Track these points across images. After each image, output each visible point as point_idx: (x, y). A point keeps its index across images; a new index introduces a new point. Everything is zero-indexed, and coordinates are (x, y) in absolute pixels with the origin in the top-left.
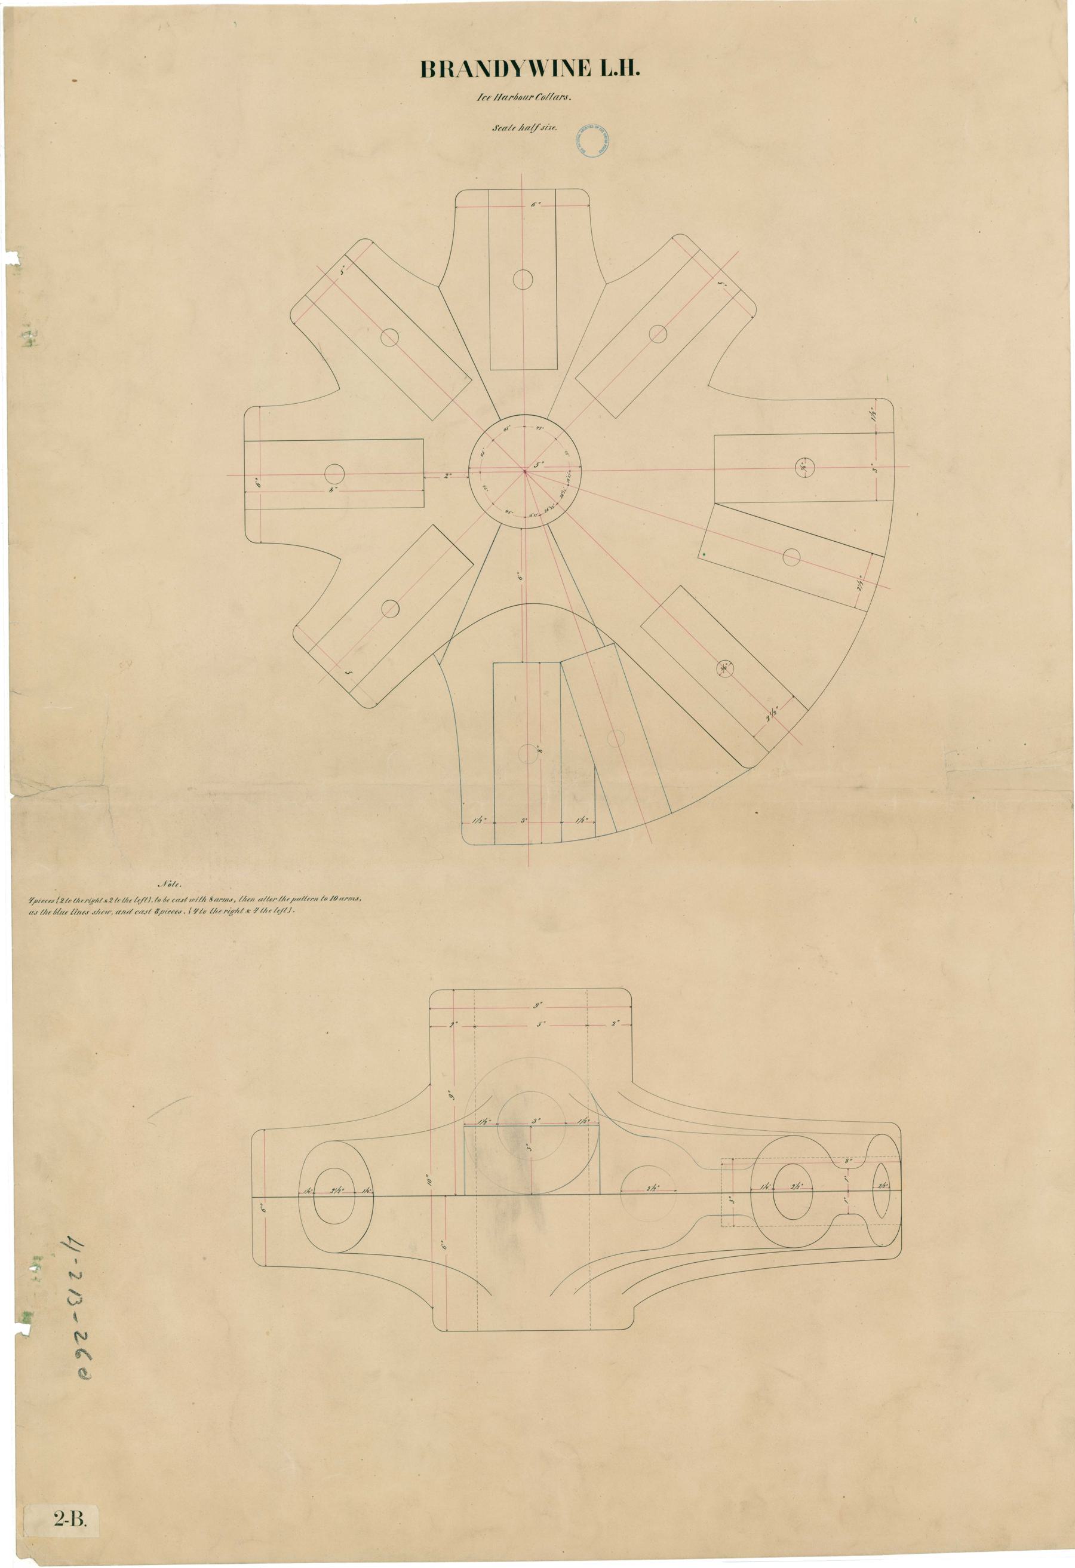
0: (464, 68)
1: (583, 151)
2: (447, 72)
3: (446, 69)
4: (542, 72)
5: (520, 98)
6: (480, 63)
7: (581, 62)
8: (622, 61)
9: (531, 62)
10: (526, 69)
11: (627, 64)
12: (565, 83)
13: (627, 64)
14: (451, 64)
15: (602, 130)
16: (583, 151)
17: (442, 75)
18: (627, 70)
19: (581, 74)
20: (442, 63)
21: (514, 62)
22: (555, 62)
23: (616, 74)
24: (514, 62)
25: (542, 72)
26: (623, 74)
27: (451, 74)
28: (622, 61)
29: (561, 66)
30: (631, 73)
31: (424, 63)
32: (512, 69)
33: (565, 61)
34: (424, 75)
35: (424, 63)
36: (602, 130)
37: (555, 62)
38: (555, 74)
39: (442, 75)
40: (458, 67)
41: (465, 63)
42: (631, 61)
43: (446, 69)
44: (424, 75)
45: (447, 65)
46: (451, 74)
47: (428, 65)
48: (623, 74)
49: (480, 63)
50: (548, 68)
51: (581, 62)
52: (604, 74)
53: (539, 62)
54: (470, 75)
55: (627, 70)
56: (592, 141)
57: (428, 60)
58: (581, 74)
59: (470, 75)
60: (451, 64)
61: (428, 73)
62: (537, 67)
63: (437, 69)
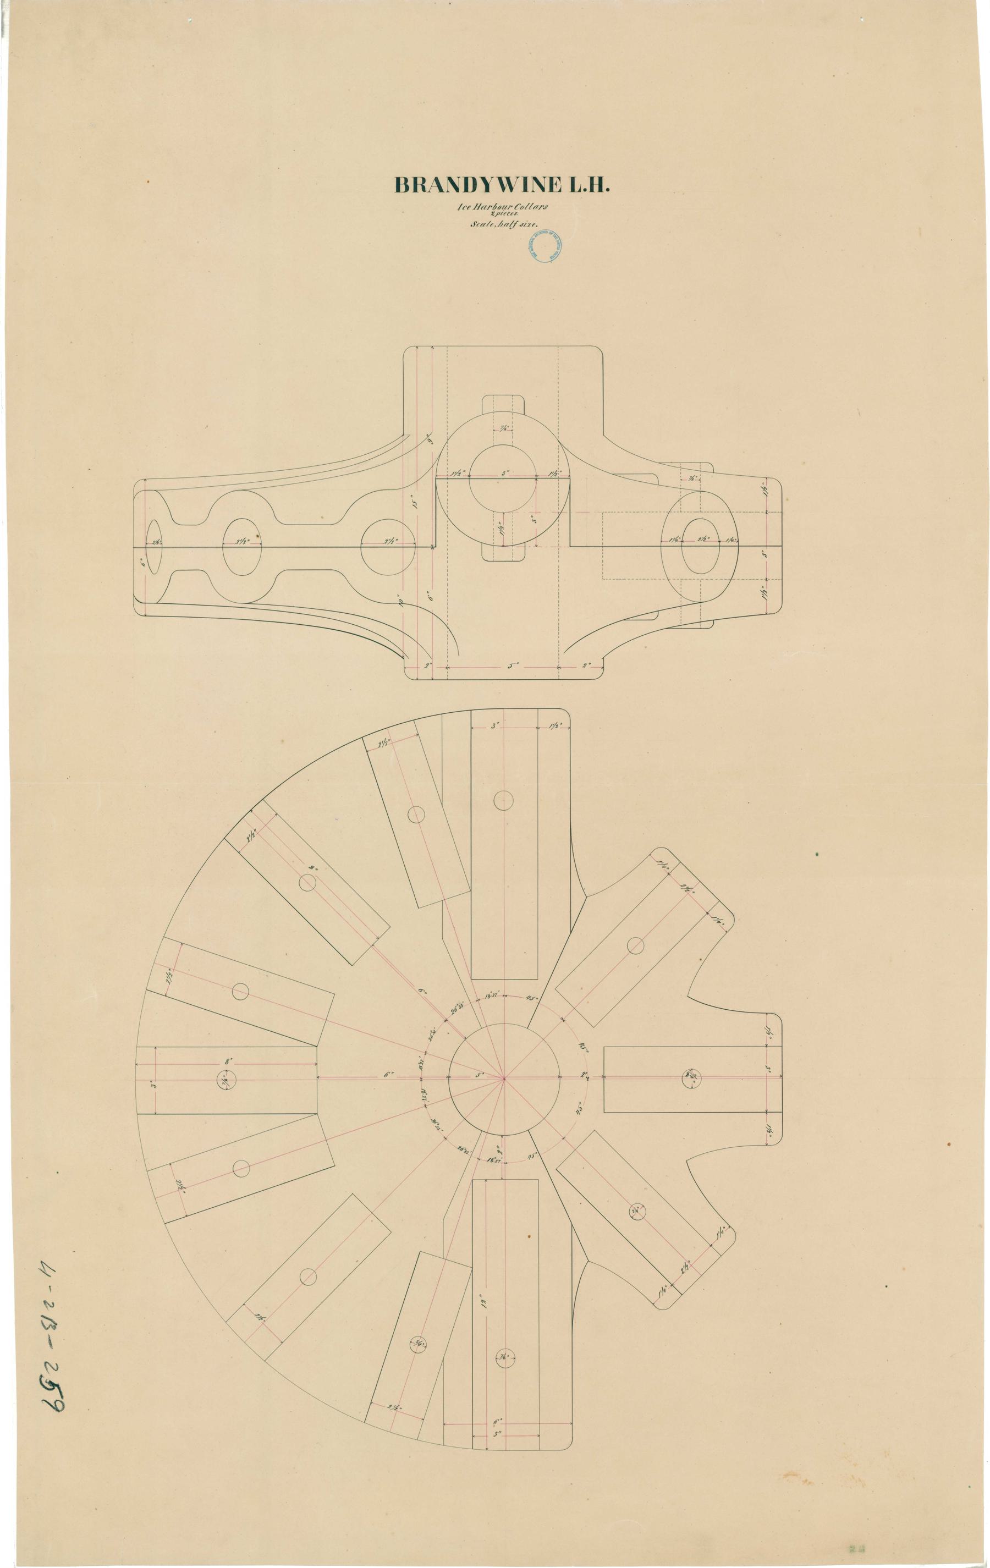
0: (435, 184)
1: (535, 255)
2: (419, 188)
3: (418, 185)
7: (551, 179)
8: (592, 179)
9: (500, 179)
10: (494, 185)
11: (596, 181)
13: (596, 181)
14: (424, 180)
15: (556, 236)
16: (535, 255)
17: (415, 190)
18: (596, 188)
19: (551, 190)
20: (415, 179)
21: (484, 179)
22: (525, 179)
23: (585, 190)
24: (484, 179)
25: (511, 189)
26: (592, 190)
27: (424, 189)
28: (592, 179)
30: (600, 190)
32: (480, 185)
34: (398, 190)
35: (398, 179)
36: (556, 236)
37: (525, 179)
38: (525, 190)
39: (415, 190)
41: (436, 179)
42: (600, 179)
43: (418, 185)
44: (398, 190)
45: (420, 181)
46: (424, 189)
47: (402, 181)
48: (592, 190)
49: (450, 179)
50: (518, 185)
51: (551, 179)
52: (573, 190)
54: (441, 190)
55: (596, 188)
58: (551, 190)
59: (441, 190)
60: (424, 180)
61: (403, 188)
62: (506, 184)
63: (411, 184)
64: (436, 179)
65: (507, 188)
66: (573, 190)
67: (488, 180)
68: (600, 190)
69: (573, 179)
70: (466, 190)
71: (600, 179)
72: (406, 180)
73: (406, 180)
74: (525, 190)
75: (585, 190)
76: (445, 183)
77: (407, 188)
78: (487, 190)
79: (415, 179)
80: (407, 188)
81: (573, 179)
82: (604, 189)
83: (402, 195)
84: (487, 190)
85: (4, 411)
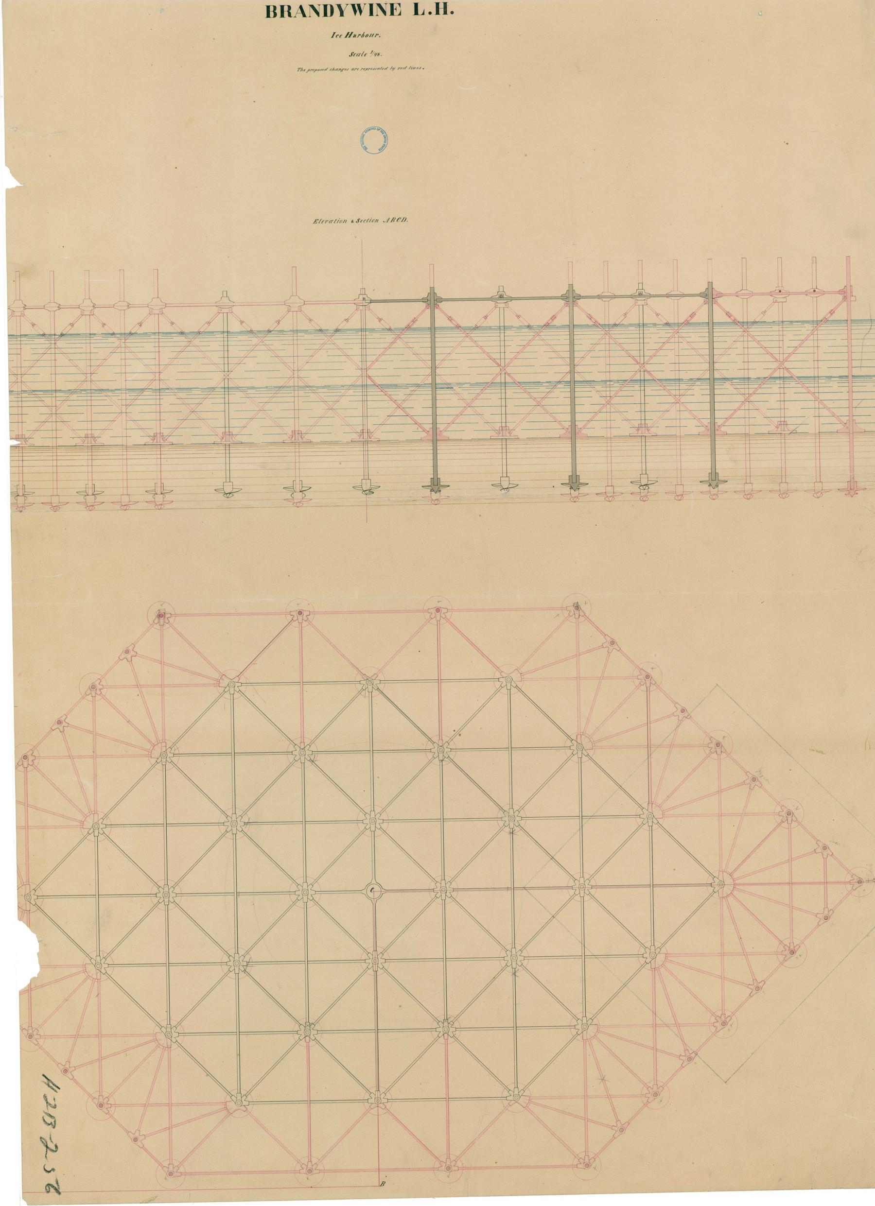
0: (300, 11)
1: (366, 148)
2: (286, 14)
3: (285, 11)
4: (361, 12)
5: (367, 36)
6: (312, 6)
7: (392, 5)
8: (437, 4)
9: (353, 5)
10: (348, 11)
11: (441, 6)
12: (380, 21)
13: (441, 6)
14: (289, 7)
15: (383, 132)
16: (366, 148)
17: (282, 16)
18: (441, 11)
19: (392, 14)
20: (282, 7)
21: (339, 6)
22: (371, 5)
23: (430, 13)
24: (339, 6)
25: (361, 12)
26: (438, 13)
27: (290, 15)
28: (437, 4)
29: (376, 8)
30: (445, 13)
31: (268, 7)
32: (337, 11)
33: (379, 5)
34: (268, 16)
35: (268, 7)
36: (383, 132)
37: (371, 5)
38: (371, 14)
39: (282, 16)
40: (295, 10)
41: (301, 7)
42: (445, 4)
43: (285, 11)
44: (268, 16)
45: (286, 9)
46: (290, 15)
47: (272, 9)
48: (438, 13)
49: (312, 6)
50: (366, 10)
51: (392, 5)
52: (416, 13)
53: (359, 5)
54: (304, 16)
55: (441, 11)
56: (374, 140)
57: (271, 3)
58: (392, 14)
59: (304, 16)
60: (289, 7)
61: (272, 14)
62: (357, 9)
63: (278, 11)
64: (301, 7)
65: (358, 12)
66: (416, 13)
67: (343, 7)
68: (445, 13)
69: (416, 5)
70: (325, 15)
71: (445, 4)
72: (275, 7)
73: (275, 7)
74: (371, 14)
75: (430, 13)
76: (307, 10)
77: (275, 15)
78: (342, 14)
79: (282, 7)
80: (275, 15)
81: (416, 5)
82: (449, 12)
83: (271, 19)
84: (342, 14)
85: (3, 99)
